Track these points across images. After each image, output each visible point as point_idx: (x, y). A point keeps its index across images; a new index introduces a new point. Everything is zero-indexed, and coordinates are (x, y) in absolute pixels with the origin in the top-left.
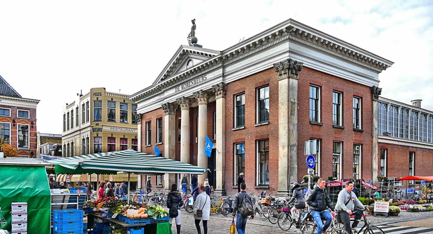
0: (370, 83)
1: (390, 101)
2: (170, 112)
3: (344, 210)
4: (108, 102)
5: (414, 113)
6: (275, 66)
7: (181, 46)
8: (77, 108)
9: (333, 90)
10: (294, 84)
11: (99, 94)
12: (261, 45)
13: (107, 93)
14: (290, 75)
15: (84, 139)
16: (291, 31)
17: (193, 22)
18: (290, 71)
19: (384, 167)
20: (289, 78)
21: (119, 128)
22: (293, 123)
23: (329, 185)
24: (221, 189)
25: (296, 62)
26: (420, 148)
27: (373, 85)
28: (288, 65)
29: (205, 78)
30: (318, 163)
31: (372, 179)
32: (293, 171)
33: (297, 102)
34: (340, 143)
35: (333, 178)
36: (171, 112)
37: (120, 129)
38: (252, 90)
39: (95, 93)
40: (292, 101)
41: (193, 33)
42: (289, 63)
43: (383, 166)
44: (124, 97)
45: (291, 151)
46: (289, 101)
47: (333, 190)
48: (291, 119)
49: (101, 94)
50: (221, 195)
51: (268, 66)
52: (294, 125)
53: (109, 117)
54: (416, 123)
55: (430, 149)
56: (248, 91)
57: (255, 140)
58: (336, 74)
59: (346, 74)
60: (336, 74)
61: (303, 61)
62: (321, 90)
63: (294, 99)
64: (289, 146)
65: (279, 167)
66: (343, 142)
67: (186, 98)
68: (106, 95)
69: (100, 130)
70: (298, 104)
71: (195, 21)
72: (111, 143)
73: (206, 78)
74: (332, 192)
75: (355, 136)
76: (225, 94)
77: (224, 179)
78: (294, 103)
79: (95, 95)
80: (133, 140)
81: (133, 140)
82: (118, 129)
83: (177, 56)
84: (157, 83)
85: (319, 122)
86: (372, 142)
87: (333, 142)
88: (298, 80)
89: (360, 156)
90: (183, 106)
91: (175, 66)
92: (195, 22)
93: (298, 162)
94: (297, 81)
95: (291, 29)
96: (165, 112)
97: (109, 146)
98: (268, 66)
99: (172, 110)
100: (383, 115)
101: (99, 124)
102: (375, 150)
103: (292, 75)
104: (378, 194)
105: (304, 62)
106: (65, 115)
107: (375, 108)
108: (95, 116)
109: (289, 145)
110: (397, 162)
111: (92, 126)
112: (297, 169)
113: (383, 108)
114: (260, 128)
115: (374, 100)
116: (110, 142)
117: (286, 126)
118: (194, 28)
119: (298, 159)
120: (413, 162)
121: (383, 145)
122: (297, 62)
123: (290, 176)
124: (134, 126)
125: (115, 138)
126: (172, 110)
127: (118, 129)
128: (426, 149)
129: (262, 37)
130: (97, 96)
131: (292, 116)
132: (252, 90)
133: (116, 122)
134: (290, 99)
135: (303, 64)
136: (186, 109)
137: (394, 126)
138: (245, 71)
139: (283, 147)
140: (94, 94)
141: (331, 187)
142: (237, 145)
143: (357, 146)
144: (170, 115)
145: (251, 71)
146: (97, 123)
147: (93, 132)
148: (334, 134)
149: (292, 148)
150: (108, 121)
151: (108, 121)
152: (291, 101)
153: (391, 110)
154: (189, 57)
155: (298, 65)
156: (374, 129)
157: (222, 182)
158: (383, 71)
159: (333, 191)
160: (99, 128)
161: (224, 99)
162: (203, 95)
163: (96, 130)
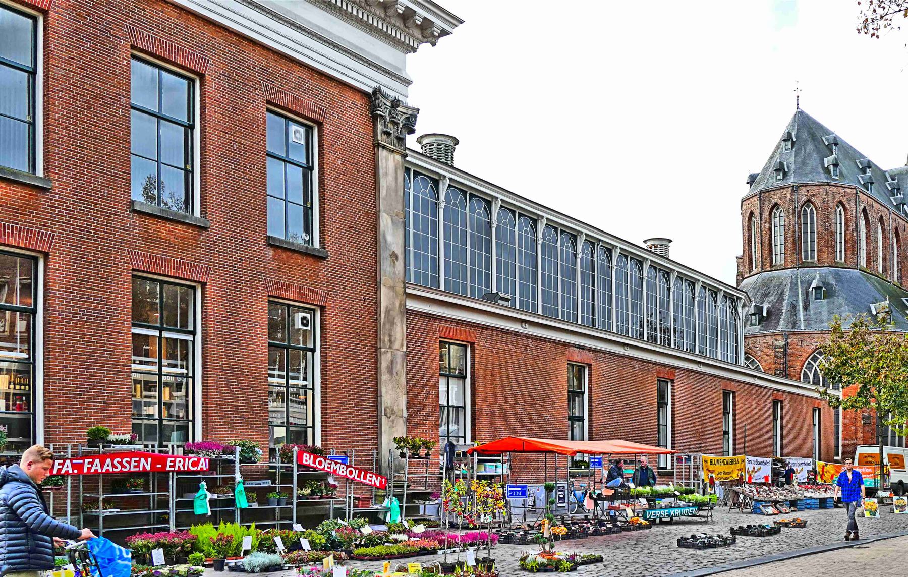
0: (367, 80)
1: (701, 277)
5: (659, 275)
9: (133, 47)
19: (464, 408)
26: (611, 354)
27: (374, 85)
30: (313, 389)
31: (378, 447)
35: (112, 437)
43: (461, 404)
47: (101, 490)
54: (723, 322)
55: (649, 362)
58: (245, 27)
59: (262, 23)
60: (245, 27)
74: (97, 500)
75: (278, 270)
85: (40, 172)
86: (376, 303)
87: (134, 276)
89: (315, 354)
100: (709, 315)
102: (390, 336)
104: (396, 503)
107: (391, 178)
110: (517, 395)
113: (660, 282)
115: (384, 147)
120: (586, 396)
121: (454, 326)
122: (399, 101)
128: (631, 358)
137: (710, 335)
143: (301, 315)
153: (678, 288)
156: (384, 255)
158: (425, 47)
159: (102, 497)
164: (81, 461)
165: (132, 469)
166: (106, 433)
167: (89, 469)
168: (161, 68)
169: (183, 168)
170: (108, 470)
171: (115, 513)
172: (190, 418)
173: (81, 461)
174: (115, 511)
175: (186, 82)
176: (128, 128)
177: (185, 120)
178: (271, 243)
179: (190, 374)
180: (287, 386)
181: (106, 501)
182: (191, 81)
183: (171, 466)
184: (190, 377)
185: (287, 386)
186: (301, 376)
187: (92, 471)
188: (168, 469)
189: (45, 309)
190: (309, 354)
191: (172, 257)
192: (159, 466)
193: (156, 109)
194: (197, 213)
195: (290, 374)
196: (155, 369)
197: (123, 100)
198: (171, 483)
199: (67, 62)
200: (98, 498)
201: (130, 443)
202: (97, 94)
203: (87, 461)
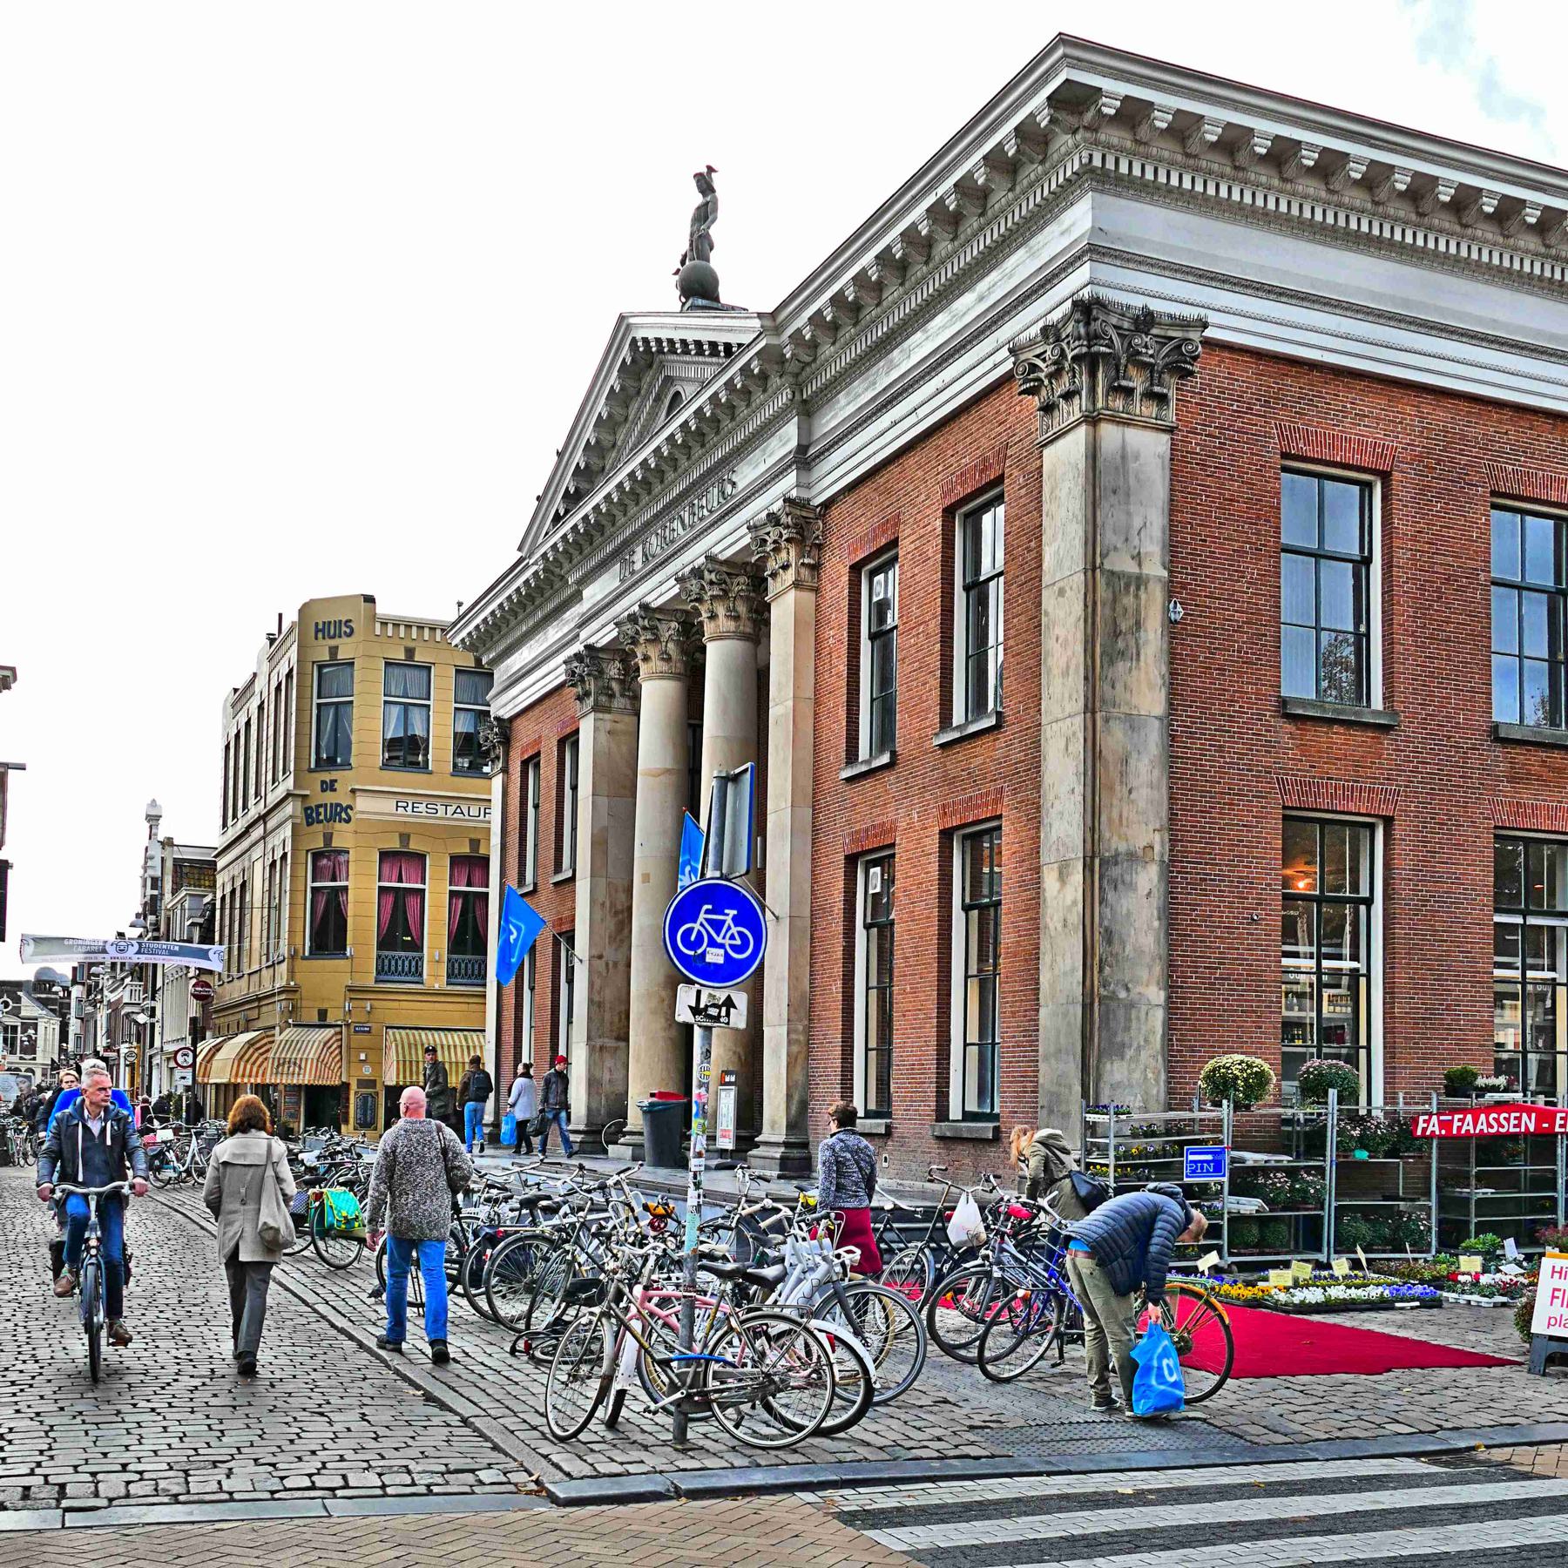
2: (603, 699)
3: (1435, 1311)
4: (390, 669)
6: (1022, 357)
7: (622, 318)
8: (261, 707)
9: (1494, 493)
10: (1137, 458)
11: (344, 629)
12: (952, 240)
13: (384, 624)
14: (1100, 405)
15: (273, 864)
16: (1089, 116)
17: (704, 183)
18: (1100, 375)
20: (1092, 420)
21: (446, 802)
22: (1124, 709)
23: (1434, 1127)
24: (782, 1138)
25: (1146, 320)
28: (1079, 338)
29: (729, 489)
30: (1368, 976)
32: (1127, 1029)
33: (1165, 574)
34: (1371, 827)
35: (1481, 1082)
36: (612, 696)
37: (451, 810)
38: (929, 528)
39: (320, 627)
40: (1117, 568)
41: (701, 245)
42: (1087, 324)
44: (408, 633)
45: (1110, 896)
46: (1094, 570)
48: (1107, 688)
49: (352, 631)
50: (775, 1173)
51: (995, 366)
52: (1133, 722)
53: (459, 753)
56: (913, 537)
57: (941, 832)
61: (1203, 312)
62: (1385, 498)
63: (1138, 558)
64: (1097, 861)
65: (1042, 1001)
66: (1388, 821)
67: (660, 609)
68: (378, 632)
69: (344, 815)
70: (1172, 590)
71: (717, 181)
72: (400, 880)
73: (734, 484)
76: (815, 568)
77: (799, 1076)
78: (1140, 581)
79: (320, 635)
80: (456, 861)
81: (456, 861)
82: (441, 809)
83: (611, 382)
84: (540, 541)
85: (1377, 702)
88: (1170, 430)
89: (1373, 908)
90: (646, 659)
91: (611, 438)
92: (716, 185)
93: (1171, 966)
94: (1165, 438)
95: (1088, 110)
96: (580, 698)
97: (390, 899)
98: (995, 366)
99: (615, 685)
101: (336, 785)
103: (1119, 403)
105: (1213, 317)
106: (227, 747)
108: (323, 744)
109: (1092, 858)
111: (304, 797)
112: (1159, 1016)
114: (960, 757)
116: (395, 876)
117: (1074, 734)
118: (705, 215)
119: (1171, 946)
123: (1099, 1061)
124: (469, 787)
125: (420, 858)
126: (615, 685)
127: (441, 809)
129: (941, 190)
130: (334, 637)
131: (1121, 666)
132: (929, 528)
133: (431, 773)
134: (1103, 556)
135: (1205, 326)
136: (662, 676)
138: (897, 418)
139: (1063, 877)
140: (317, 631)
141: (1449, 1137)
142: (872, 870)
144: (600, 715)
145: (922, 412)
146: (327, 777)
147: (309, 824)
148: (1505, 786)
149: (1115, 872)
150: (386, 766)
151: (386, 766)
152: (1107, 566)
154: (669, 380)
155: (1171, 339)
157: (789, 1097)
160: (338, 805)
161: (809, 597)
162: (722, 582)
163: (322, 817)
164: (1450, 1118)
165: (1512, 1130)
166: (1475, 1076)
167: (1459, 1128)
168: (1524, 512)
169: (1351, 629)
170: (1482, 1130)
171: (1489, 1196)
172: (1363, 1042)
173: (1450, 1118)
174: (1488, 1192)
175: (1356, 489)
176: (1488, 616)
177: (1356, 551)
178: (1496, 735)
179: (1363, 971)
180: (1524, 982)
181: (1479, 1176)
182: (1366, 487)
183: (1561, 1126)
184: (1363, 975)
185: (1524, 982)
186: (1346, 951)
187: (1463, 1132)
188: (1557, 1129)
189: (1387, 897)
190: (1363, 908)
191: (1297, 775)
192: (1546, 1125)
193: (1515, 574)
194: (1377, 702)
195: (1324, 950)
196: (1517, 974)
197: (1482, 577)
198: (1559, 1150)
199: (1414, 539)
200: (1468, 1172)
201: (1506, 1090)
202: (1450, 575)
203: (1457, 1117)
